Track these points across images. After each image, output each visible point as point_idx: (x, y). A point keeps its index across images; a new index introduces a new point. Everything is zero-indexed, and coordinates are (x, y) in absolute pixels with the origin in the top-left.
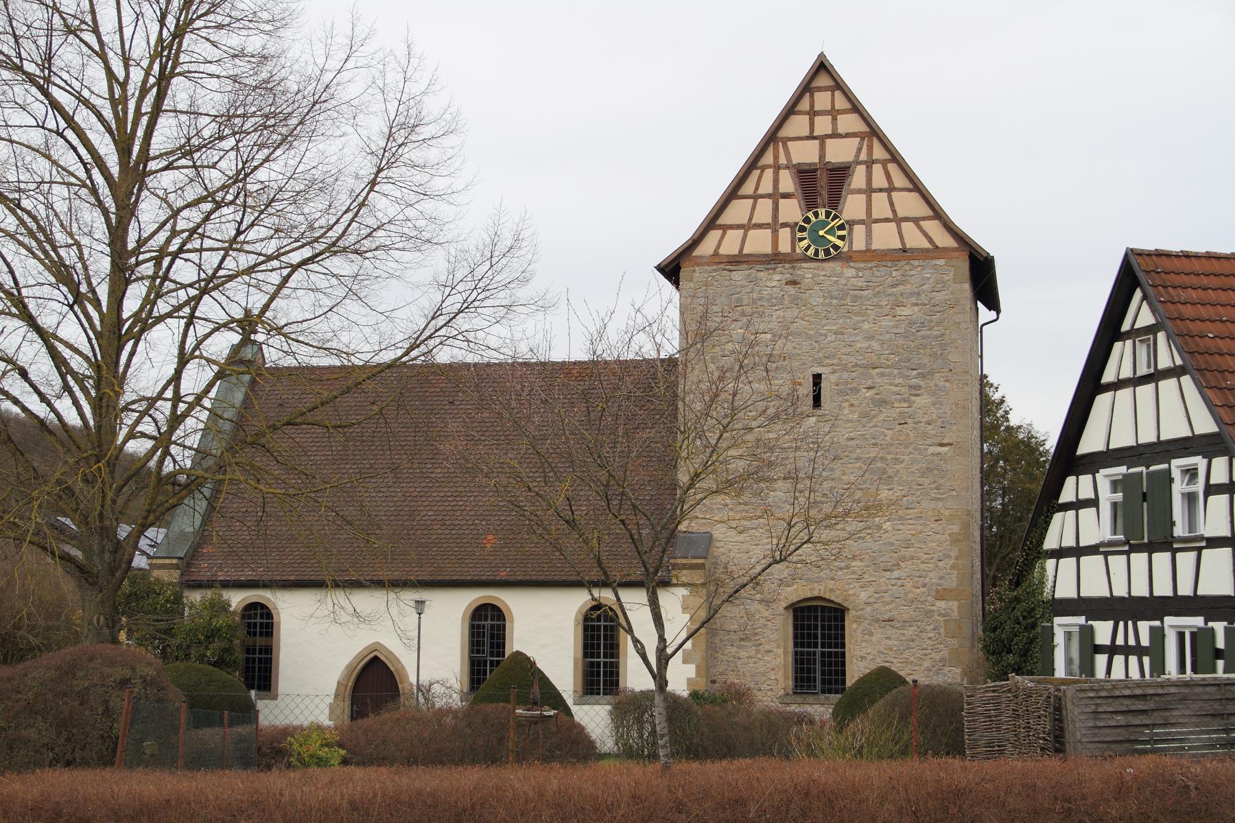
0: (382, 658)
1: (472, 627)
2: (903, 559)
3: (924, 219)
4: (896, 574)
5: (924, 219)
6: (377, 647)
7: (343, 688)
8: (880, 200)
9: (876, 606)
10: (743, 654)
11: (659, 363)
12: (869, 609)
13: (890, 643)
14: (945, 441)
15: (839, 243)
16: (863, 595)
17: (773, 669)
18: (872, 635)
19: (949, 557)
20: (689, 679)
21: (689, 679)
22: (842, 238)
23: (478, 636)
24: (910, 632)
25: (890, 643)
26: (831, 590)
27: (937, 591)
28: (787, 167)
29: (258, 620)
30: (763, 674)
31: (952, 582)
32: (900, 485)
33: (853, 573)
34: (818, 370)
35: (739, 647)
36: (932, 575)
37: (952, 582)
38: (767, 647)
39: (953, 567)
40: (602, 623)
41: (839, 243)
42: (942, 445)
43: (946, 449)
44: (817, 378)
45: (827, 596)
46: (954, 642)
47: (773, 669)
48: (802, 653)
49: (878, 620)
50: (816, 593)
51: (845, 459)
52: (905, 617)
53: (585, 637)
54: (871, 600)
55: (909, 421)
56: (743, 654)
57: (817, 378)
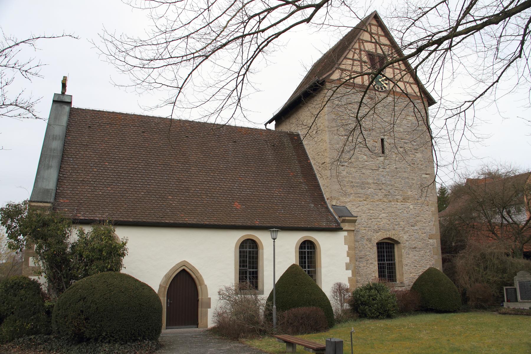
0: (188, 270)
1: (240, 252)
2: (417, 221)
3: (412, 83)
4: (416, 228)
5: (412, 83)
6: (184, 263)
7: (163, 289)
8: (398, 71)
9: (410, 242)
10: (361, 265)
11: (443, 212)
12: (407, 243)
13: (416, 258)
14: (427, 173)
15: (385, 85)
16: (405, 237)
17: (374, 272)
18: (409, 254)
19: (432, 221)
20: (349, 278)
21: (349, 278)
22: (386, 84)
23: (243, 257)
24: (422, 252)
25: (416, 258)
26: (394, 235)
27: (429, 235)
28: (364, 51)
29: (248, 250)
30: (370, 274)
31: (434, 232)
32: (414, 189)
33: (401, 227)
34: (382, 137)
35: (359, 262)
36: (427, 228)
37: (434, 232)
38: (371, 261)
39: (434, 225)
40: (306, 250)
41: (385, 85)
42: (426, 174)
43: (428, 176)
44: (382, 140)
45: (392, 237)
46: (436, 257)
47: (374, 272)
48: (381, 264)
49: (411, 248)
50: (388, 236)
51: (395, 177)
52: (420, 246)
53: (240, 256)
54: (408, 239)
55: (416, 163)
56: (361, 265)
57: (382, 140)
